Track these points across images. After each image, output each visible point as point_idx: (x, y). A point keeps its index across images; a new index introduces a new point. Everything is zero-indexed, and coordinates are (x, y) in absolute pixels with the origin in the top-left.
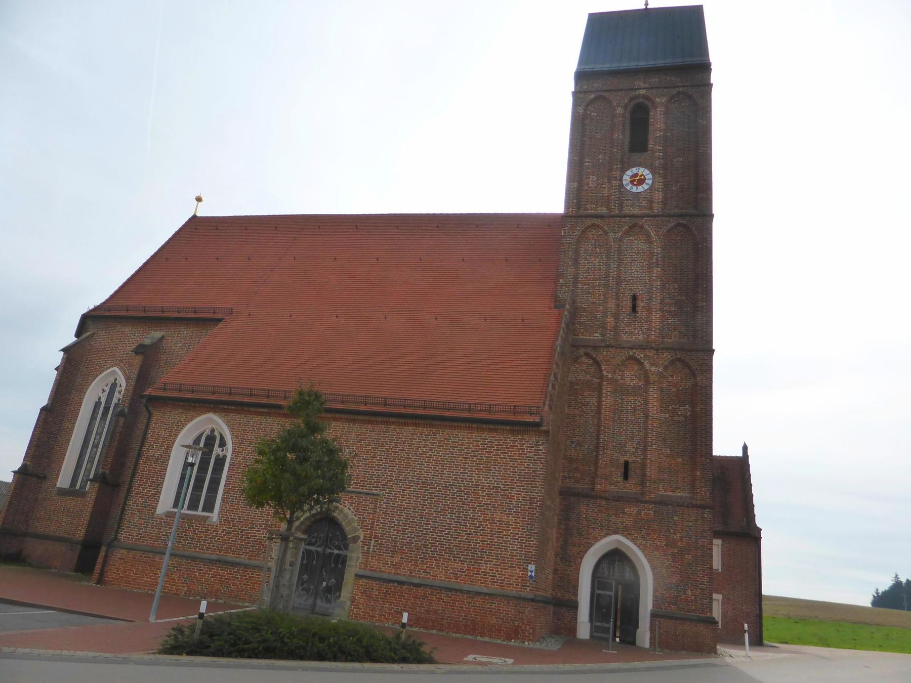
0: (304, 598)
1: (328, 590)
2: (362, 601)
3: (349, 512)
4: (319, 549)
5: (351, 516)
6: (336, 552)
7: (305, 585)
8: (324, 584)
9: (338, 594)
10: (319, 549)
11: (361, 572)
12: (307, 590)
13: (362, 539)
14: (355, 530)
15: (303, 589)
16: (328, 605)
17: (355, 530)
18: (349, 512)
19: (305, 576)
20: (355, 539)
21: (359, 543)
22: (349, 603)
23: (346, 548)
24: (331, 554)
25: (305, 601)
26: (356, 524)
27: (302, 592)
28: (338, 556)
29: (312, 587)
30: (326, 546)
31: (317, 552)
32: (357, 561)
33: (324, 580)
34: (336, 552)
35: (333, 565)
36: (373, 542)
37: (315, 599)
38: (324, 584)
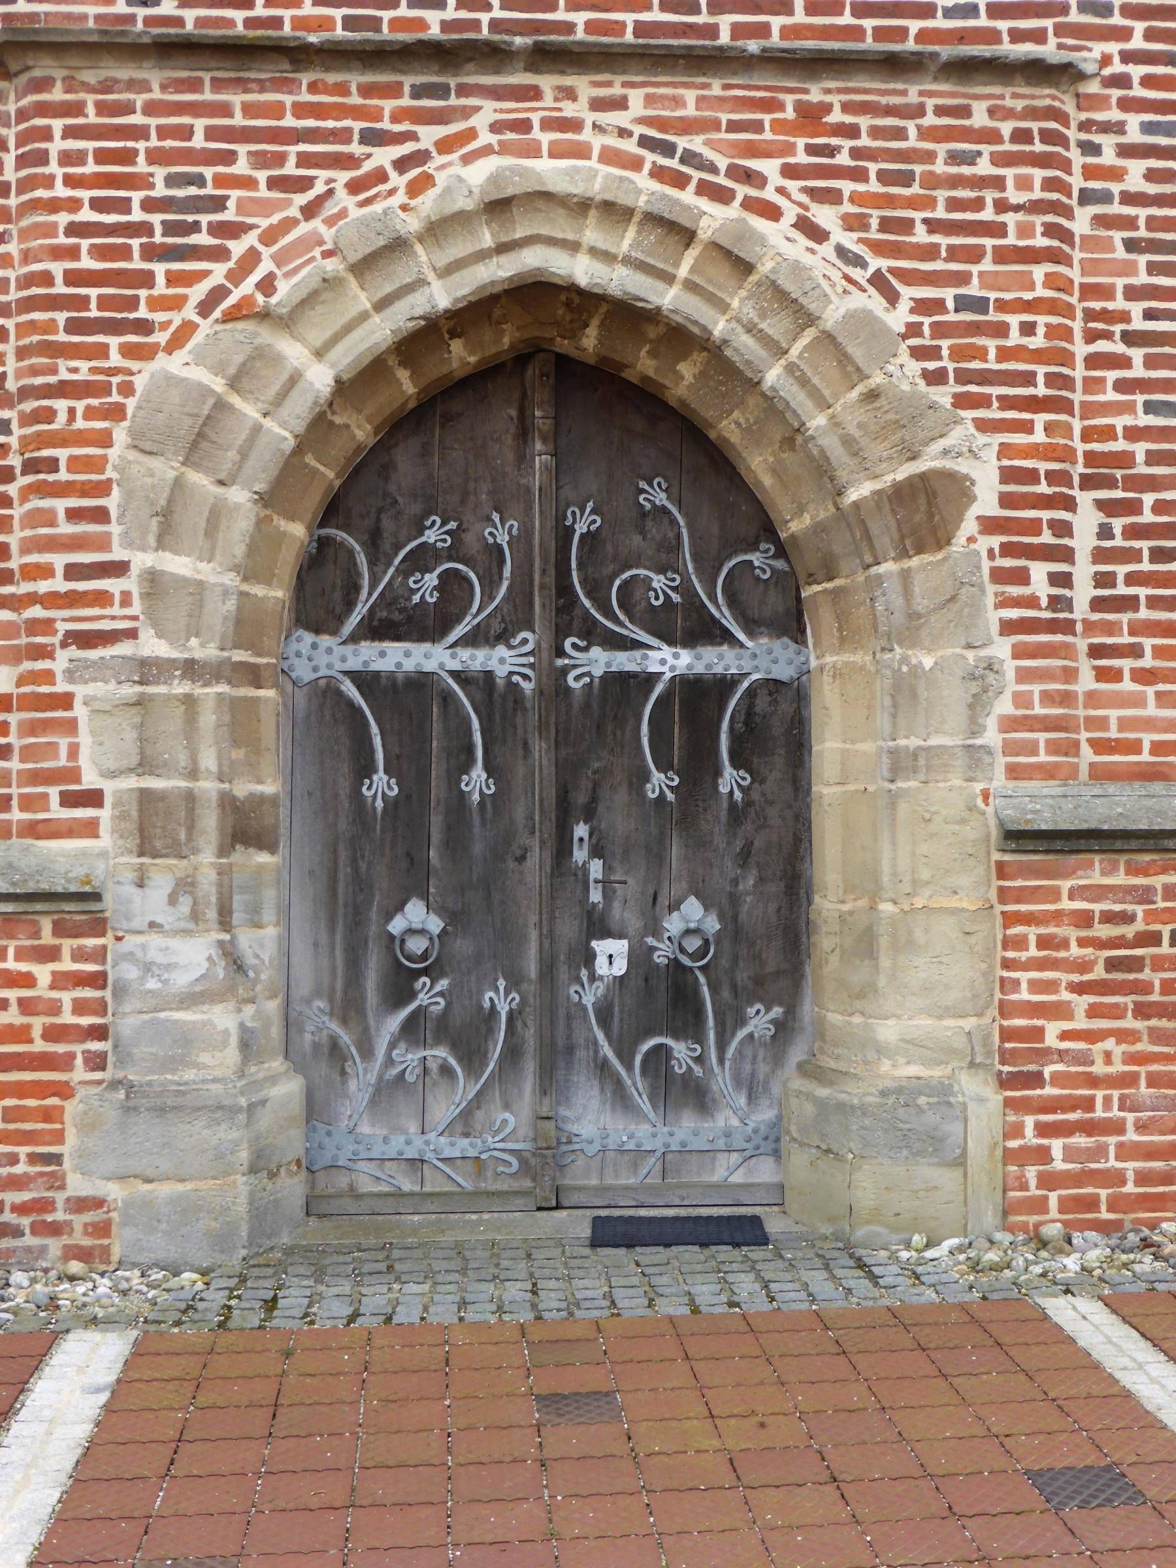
0: (444, 1107)
1: (667, 998)
2: (1108, 1059)
3: (819, 261)
4: (500, 660)
5: (842, 304)
6: (668, 661)
7: (429, 995)
8: (612, 956)
9: (760, 1021)
10: (500, 660)
11: (1045, 805)
12: (466, 1036)
13: (987, 503)
14: (905, 427)
15: (412, 1030)
16: (688, 1127)
17: (905, 427)
18: (819, 261)
19: (415, 913)
20: (924, 510)
21: (972, 543)
22: (981, 1099)
23: (334, 723)
24: (626, 688)
25: (464, 1123)
26: (906, 371)
27: (409, 1058)
28: (699, 696)
29: (500, 1000)
30: (569, 621)
31: (481, 684)
32: (977, 706)
33: (599, 925)
34: (668, 661)
35: (659, 782)
36: (1086, 520)
37: (551, 1081)
38: (612, 956)
